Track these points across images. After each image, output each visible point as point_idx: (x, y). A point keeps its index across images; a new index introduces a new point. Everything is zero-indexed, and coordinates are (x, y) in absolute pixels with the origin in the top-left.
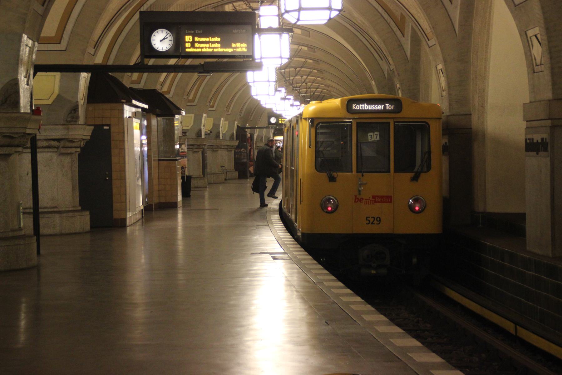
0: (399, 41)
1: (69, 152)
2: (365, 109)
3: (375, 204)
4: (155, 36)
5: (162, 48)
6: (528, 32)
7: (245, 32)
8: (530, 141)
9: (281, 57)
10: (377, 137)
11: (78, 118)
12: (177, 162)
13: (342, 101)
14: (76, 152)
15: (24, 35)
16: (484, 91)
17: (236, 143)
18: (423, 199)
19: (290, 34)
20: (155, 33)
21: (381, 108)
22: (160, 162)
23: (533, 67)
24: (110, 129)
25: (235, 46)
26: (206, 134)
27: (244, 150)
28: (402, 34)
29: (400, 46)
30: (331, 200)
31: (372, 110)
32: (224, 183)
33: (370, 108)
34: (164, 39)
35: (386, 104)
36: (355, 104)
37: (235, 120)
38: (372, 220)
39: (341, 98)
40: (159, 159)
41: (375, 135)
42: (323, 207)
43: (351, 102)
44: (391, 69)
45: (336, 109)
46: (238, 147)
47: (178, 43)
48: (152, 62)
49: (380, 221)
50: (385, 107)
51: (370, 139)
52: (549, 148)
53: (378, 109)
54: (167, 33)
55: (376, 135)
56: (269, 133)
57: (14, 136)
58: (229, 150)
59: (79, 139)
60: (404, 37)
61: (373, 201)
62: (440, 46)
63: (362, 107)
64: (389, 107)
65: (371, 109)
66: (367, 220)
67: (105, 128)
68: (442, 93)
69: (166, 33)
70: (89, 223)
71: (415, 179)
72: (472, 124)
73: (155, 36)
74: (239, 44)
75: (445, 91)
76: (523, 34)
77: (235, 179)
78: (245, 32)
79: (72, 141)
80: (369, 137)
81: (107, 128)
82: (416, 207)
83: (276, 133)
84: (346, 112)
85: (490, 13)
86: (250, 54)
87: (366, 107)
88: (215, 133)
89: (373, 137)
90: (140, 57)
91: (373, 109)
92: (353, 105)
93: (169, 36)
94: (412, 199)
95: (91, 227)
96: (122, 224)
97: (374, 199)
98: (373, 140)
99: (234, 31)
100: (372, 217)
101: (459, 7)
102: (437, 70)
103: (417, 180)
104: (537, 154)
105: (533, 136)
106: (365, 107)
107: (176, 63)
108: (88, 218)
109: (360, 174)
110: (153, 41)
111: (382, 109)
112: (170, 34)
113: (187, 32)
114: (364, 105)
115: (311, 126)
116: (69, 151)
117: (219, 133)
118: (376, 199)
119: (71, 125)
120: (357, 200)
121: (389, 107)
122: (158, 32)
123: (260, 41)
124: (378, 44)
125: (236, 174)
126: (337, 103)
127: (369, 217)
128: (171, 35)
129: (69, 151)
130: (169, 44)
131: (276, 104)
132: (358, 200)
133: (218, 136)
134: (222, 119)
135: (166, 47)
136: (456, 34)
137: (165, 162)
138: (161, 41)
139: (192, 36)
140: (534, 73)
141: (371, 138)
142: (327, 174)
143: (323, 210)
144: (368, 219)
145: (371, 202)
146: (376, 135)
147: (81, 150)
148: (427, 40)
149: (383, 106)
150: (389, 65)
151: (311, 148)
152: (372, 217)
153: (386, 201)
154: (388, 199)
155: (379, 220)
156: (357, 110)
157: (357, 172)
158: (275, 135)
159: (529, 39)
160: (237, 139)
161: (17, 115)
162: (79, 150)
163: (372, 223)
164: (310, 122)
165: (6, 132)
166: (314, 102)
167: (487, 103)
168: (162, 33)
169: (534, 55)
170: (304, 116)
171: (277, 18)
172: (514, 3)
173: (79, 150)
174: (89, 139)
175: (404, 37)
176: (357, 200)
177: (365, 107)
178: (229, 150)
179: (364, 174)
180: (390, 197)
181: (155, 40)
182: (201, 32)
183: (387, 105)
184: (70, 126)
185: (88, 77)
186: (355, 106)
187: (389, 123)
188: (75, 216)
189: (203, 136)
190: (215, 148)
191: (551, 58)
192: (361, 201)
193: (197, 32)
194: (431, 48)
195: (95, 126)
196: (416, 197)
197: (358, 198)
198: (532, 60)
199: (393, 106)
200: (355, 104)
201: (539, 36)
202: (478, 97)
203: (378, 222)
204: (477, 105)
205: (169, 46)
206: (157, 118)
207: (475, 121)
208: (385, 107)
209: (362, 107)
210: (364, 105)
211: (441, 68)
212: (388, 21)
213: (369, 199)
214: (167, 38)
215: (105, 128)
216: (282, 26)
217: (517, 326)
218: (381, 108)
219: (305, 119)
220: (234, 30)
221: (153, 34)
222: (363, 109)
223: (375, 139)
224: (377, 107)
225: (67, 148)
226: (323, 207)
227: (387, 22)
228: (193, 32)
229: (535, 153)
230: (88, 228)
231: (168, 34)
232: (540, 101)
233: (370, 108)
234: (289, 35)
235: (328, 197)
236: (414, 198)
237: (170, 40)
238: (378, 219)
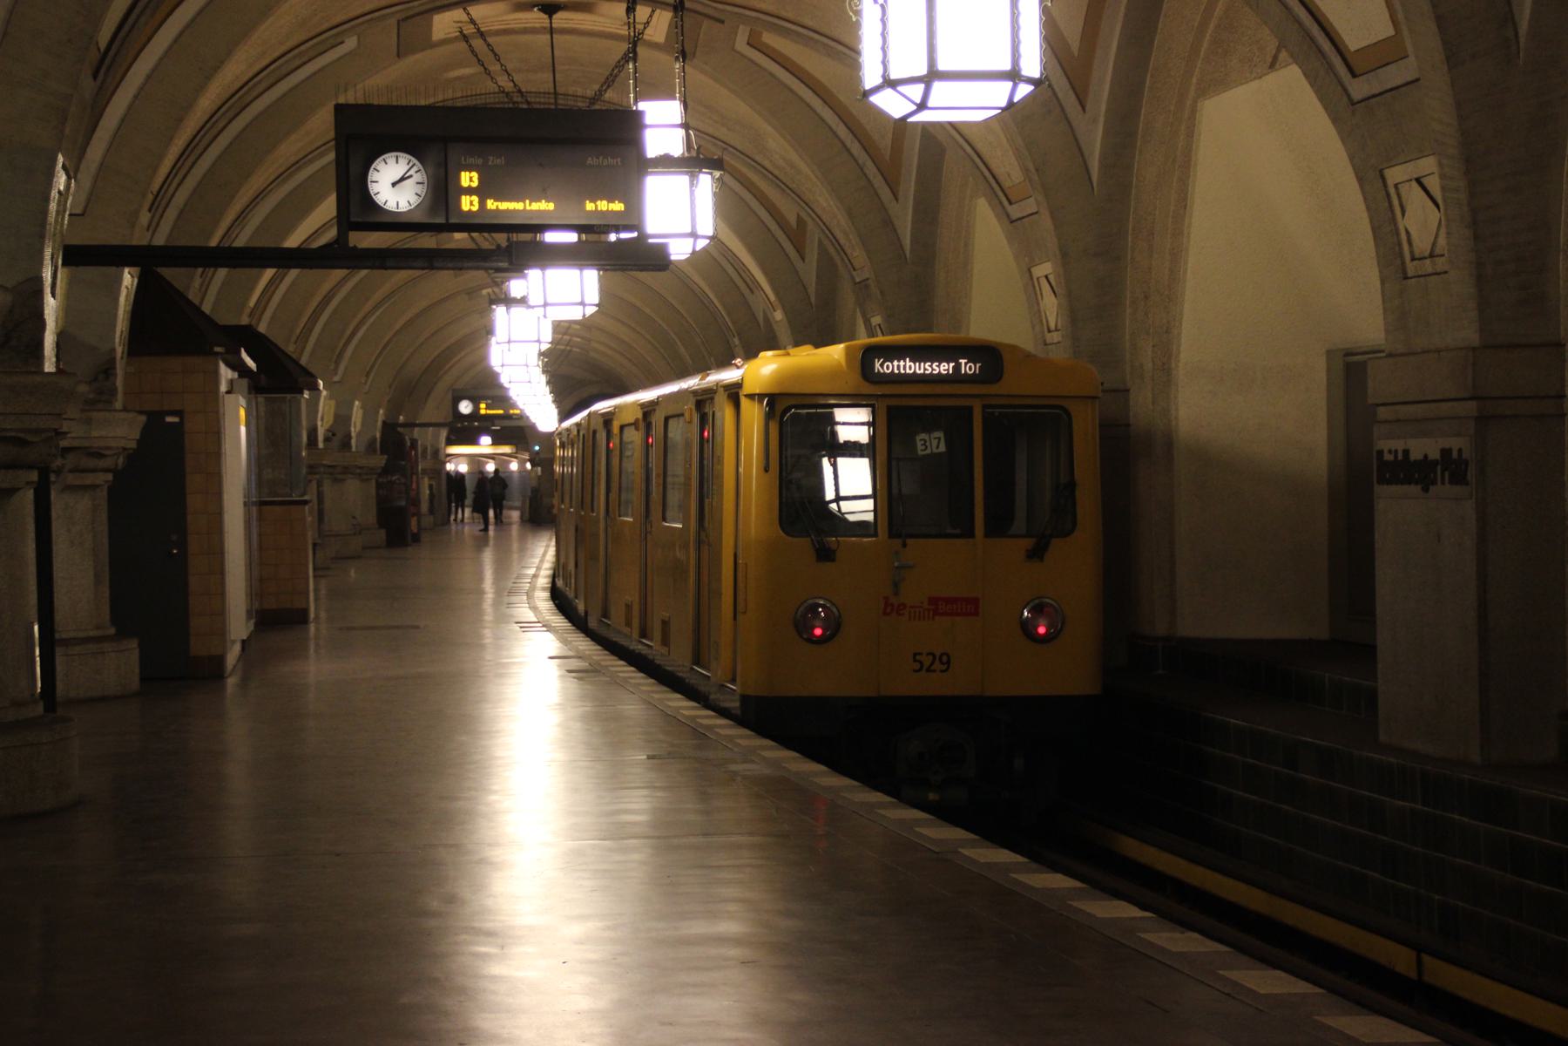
0: (885, 210)
1: (88, 482)
2: (908, 371)
3: (937, 618)
4: (378, 171)
6: (1388, 173)
7: (619, 163)
8: (1396, 457)
9: (582, 304)
10: (939, 443)
11: (113, 392)
12: (307, 507)
13: (848, 351)
16: (1168, 331)
17: (380, 461)
18: (1055, 604)
19: (717, 174)
20: (378, 164)
21: (948, 370)
22: (264, 508)
23: (1403, 263)
24: (182, 422)
25: (594, 209)
26: (327, 440)
27: (398, 479)
29: (888, 223)
30: (820, 610)
31: (924, 374)
32: (359, 557)
34: (402, 179)
35: (961, 361)
36: (882, 360)
37: (379, 407)
38: (937, 665)
39: (847, 344)
40: (262, 499)
41: (935, 438)
42: (802, 626)
43: (871, 353)
44: (858, 280)
45: (833, 373)
46: (386, 471)
47: (442, 191)
49: (948, 662)
50: (957, 368)
51: (922, 450)
52: (1471, 474)
54: (411, 165)
55: (937, 440)
56: (436, 437)
57: (29, 438)
58: (365, 477)
59: (118, 448)
60: (897, 199)
61: (931, 613)
62: (1053, 218)
63: (899, 367)
64: (967, 367)
65: (922, 371)
66: (915, 661)
67: (169, 419)
68: (1043, 336)
69: (408, 164)
70: (137, 670)
71: (1037, 553)
72: (1131, 414)
73: (378, 171)
74: (605, 202)
75: (1057, 330)
76: (1371, 176)
77: (379, 547)
78: (619, 163)
79: (100, 456)
80: (920, 446)
81: (176, 420)
82: (1039, 626)
83: (453, 438)
84: (861, 379)
85: (1190, 134)
88: (339, 435)
89: (928, 444)
90: (1000, 111)
91: (927, 372)
92: (876, 360)
93: (416, 172)
94: (1029, 607)
95: (143, 679)
96: (213, 670)
98: (929, 451)
99: (589, 161)
100: (928, 654)
101: (1102, 119)
102: (1032, 279)
103: (1041, 558)
104: (1426, 490)
105: (1406, 443)
106: (907, 367)
107: (213, 275)
108: (135, 656)
109: (898, 542)
111: (951, 372)
112: (419, 165)
113: (465, 160)
114: (905, 361)
115: (769, 416)
116: (89, 479)
117: (349, 436)
118: (939, 606)
119: (100, 410)
120: (889, 610)
121: (967, 367)
122: (387, 161)
124: (824, 218)
125: (382, 534)
126: (836, 357)
127: (920, 654)
128: (421, 168)
129: (89, 479)
130: (417, 194)
131: (527, 366)
132: (892, 608)
133: (346, 444)
134: (357, 403)
136: (1093, 188)
137: (277, 509)
138: (394, 185)
139: (477, 172)
140: (1406, 278)
141: (923, 447)
142: (812, 540)
143: (801, 637)
144: (918, 657)
145: (926, 613)
146: (937, 440)
147: (114, 477)
148: (1006, 203)
149: (952, 365)
151: (770, 472)
152: (928, 654)
153: (959, 610)
154: (969, 606)
155: (946, 661)
156: (884, 373)
157: (891, 535)
158: (450, 442)
159: (1392, 191)
160: (382, 453)
161: (38, 379)
162: (110, 477)
163: (928, 670)
164: (767, 404)
165: (9, 427)
166: (770, 353)
167: (1179, 361)
168: (397, 162)
169: (1407, 232)
170: (748, 388)
171: (682, 132)
172: (1349, 96)
173: (110, 477)
174: (134, 449)
175: (897, 199)
176: (889, 610)
177: (907, 367)
178: (365, 477)
179: (909, 541)
180: (974, 602)
181: (376, 182)
182: (503, 162)
183: (963, 361)
184: (95, 415)
185: (132, 285)
186: (882, 365)
187: (970, 409)
188: (103, 653)
189: (321, 445)
190: (339, 474)
191: (1476, 237)
192: (901, 612)
193: (493, 162)
194: (1015, 224)
195: (150, 414)
196: (1037, 601)
197: (892, 605)
198: (1400, 245)
199: (978, 365)
200: (882, 360)
201: (1051, 278)
202: (1154, 346)
203: (944, 667)
204: (1149, 366)
205: (417, 197)
206: (256, 398)
207: (1141, 404)
208: (957, 368)
209: (899, 367)
210: (905, 361)
211: (1050, 271)
212: (860, 162)
213: (921, 607)
214: (411, 176)
215: (169, 419)
216: (698, 153)
217: (1426, 958)
218: (948, 370)
219: (751, 396)
220: (590, 159)
221: (383, 157)
222: (902, 371)
223: (935, 451)
224: (938, 366)
225: (83, 471)
226: (802, 626)
227: (858, 164)
228: (480, 161)
229: (1414, 489)
230: (135, 682)
231: (414, 165)
232: (1438, 351)
234: (713, 178)
235: (810, 602)
236: (1031, 604)
237: (418, 183)
238: (945, 659)
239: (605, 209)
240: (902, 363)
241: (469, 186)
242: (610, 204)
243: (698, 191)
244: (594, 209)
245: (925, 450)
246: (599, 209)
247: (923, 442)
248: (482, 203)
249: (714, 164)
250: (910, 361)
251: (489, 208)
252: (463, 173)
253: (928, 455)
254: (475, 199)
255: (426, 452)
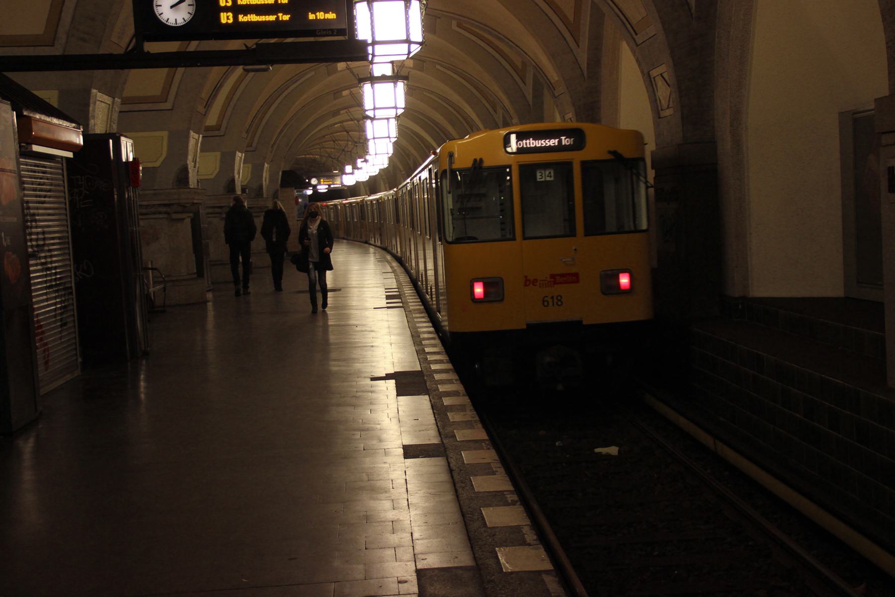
2: (532, 146)
3: (556, 286)
4: (162, 14)
5: (176, 20)
9: (396, 108)
14: (189, 217)
15: (191, 131)
19: (405, 82)
25: (314, 18)
28: (576, 41)
33: (538, 144)
35: (562, 138)
48: (153, 47)
49: (544, 302)
50: (560, 142)
51: (540, 179)
53: (550, 145)
63: (526, 143)
64: (565, 141)
65: (540, 145)
73: (162, 14)
74: (322, 13)
86: (344, 26)
87: (533, 144)
89: (543, 175)
91: (542, 145)
97: (553, 280)
98: (543, 179)
110: (158, 7)
114: (530, 140)
120: (528, 283)
121: (565, 141)
123: (373, 91)
130: (189, 13)
135: (183, 19)
138: (172, 7)
141: (540, 177)
149: (557, 140)
150: (553, 89)
180: (576, 275)
183: (563, 138)
192: (535, 284)
197: (529, 280)
199: (572, 139)
201: (665, 75)
208: (560, 142)
209: (526, 143)
210: (530, 140)
222: (528, 146)
233: (538, 144)
237: (189, 5)
239: (322, 18)
240: (528, 141)
241: (226, 6)
242: (326, 15)
243: (397, 89)
244: (314, 18)
245: (541, 178)
246: (318, 18)
247: (540, 174)
248: (235, 18)
249: (405, 78)
250: (533, 140)
251: (240, 21)
252: (222, 14)
253: (542, 181)
254: (230, 14)
255: (262, 189)
